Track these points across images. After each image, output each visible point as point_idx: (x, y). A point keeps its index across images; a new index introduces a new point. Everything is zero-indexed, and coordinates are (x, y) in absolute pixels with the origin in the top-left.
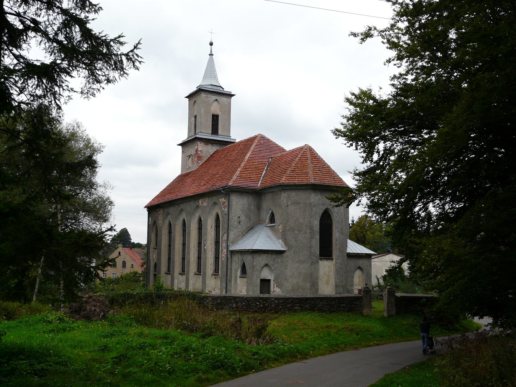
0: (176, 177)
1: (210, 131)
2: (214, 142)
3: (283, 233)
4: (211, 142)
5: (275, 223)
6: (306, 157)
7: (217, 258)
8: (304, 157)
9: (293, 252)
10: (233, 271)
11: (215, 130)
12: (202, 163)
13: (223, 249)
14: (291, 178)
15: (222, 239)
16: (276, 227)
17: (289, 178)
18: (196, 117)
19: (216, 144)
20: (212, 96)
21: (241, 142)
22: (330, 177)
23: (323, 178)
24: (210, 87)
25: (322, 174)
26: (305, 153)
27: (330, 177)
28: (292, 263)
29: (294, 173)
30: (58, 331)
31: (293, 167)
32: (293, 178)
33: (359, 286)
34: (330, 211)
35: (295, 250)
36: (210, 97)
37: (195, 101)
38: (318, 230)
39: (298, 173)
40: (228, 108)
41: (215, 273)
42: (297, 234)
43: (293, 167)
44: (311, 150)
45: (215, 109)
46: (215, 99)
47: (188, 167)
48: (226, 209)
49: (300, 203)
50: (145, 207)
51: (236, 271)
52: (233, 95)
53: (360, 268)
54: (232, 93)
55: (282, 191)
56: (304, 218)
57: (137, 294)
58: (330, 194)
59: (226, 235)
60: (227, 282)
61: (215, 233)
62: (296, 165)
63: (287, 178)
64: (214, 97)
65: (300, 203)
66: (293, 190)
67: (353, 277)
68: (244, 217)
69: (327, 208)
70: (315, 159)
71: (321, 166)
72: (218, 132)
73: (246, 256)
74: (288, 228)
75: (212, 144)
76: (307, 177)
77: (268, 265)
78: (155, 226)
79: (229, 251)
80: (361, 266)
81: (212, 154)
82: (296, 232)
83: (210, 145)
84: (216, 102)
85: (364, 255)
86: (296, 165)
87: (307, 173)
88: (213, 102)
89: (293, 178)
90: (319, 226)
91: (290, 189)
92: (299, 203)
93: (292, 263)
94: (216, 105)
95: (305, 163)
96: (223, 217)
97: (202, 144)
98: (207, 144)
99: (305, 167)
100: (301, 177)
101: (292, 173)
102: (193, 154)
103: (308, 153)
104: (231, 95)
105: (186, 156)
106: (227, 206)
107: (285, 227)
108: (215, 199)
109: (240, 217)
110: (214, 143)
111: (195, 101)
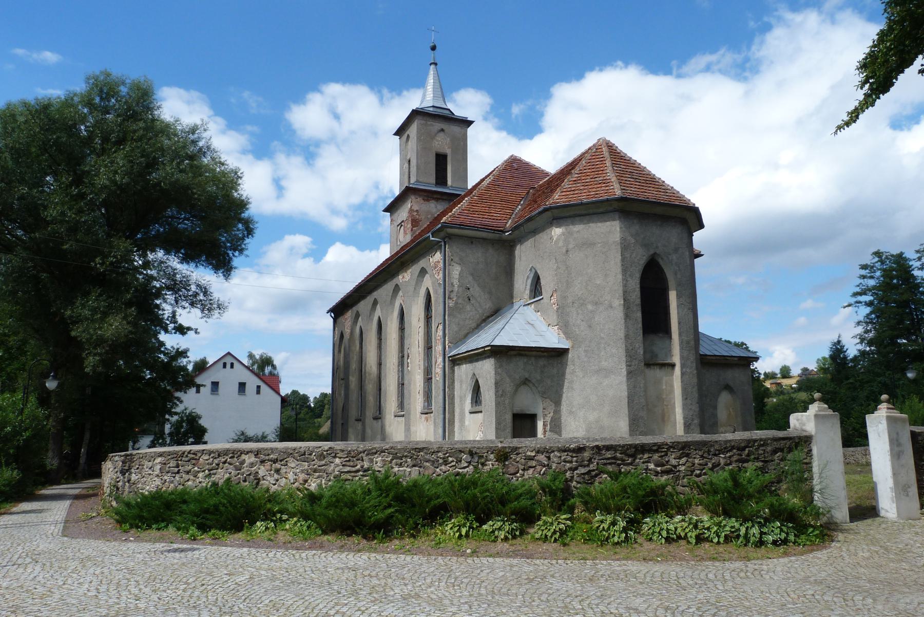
1: (433, 180)
2: (439, 197)
3: (560, 311)
4: (435, 196)
6: (602, 156)
7: (428, 380)
8: (597, 157)
9: (586, 351)
10: (457, 401)
11: (441, 178)
12: (419, 231)
13: (438, 356)
14: (572, 193)
17: (568, 193)
18: (409, 161)
19: (443, 200)
20: (434, 123)
22: (657, 190)
23: (642, 190)
24: (431, 109)
27: (657, 190)
31: (577, 175)
32: (576, 192)
34: (662, 259)
35: (589, 346)
36: (433, 126)
37: (408, 136)
38: (638, 301)
39: (586, 184)
40: (462, 143)
41: (426, 411)
42: (592, 312)
43: (577, 175)
44: (611, 148)
45: (442, 144)
48: (441, 275)
49: (594, 244)
51: (462, 399)
53: (728, 388)
55: (555, 221)
56: (606, 276)
57: (563, 492)
59: (441, 327)
60: (448, 423)
61: (426, 330)
62: (581, 172)
63: (564, 194)
64: (438, 125)
65: (594, 244)
66: (577, 218)
67: (715, 408)
68: (478, 289)
69: (655, 253)
73: (479, 364)
74: (570, 300)
75: (437, 200)
76: (607, 188)
77: (529, 381)
79: (447, 359)
80: (731, 384)
81: (436, 215)
82: (590, 307)
84: (441, 134)
85: (736, 359)
86: (581, 172)
87: (606, 182)
88: (436, 135)
89: (576, 192)
90: (639, 292)
91: (570, 217)
92: (592, 244)
93: (583, 377)
94: (442, 137)
95: (601, 166)
97: (418, 200)
98: (428, 200)
99: (600, 172)
100: (594, 190)
103: (605, 149)
104: (468, 123)
107: (565, 298)
109: (469, 289)
110: (440, 199)
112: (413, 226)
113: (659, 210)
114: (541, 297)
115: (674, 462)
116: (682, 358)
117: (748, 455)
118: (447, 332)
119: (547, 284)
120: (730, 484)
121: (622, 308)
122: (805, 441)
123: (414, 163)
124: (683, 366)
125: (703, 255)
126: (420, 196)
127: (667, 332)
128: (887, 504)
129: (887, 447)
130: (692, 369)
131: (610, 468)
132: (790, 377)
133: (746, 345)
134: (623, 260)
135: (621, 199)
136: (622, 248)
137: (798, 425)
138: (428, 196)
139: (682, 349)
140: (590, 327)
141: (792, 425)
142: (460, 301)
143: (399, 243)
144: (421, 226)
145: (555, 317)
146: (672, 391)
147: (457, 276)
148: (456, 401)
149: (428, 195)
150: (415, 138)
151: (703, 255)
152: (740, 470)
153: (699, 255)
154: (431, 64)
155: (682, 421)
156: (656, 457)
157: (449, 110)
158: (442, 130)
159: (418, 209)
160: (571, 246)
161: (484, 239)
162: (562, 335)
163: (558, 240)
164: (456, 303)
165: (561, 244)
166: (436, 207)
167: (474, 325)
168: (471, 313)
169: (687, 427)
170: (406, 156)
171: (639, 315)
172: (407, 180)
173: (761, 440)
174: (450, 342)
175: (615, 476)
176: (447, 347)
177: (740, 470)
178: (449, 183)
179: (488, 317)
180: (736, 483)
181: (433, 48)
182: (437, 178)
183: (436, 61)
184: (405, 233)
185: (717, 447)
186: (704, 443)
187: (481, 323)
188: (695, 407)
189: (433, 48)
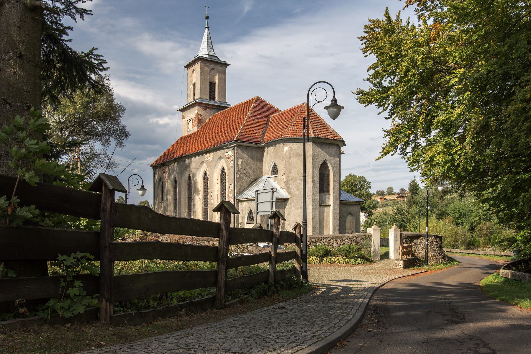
0: (178, 140)
1: (208, 97)
2: (212, 107)
5: (277, 174)
13: (230, 198)
15: (228, 190)
16: (279, 177)
20: (209, 65)
21: (237, 107)
24: (207, 56)
25: (320, 129)
26: (304, 110)
28: (295, 210)
29: (295, 128)
30: (396, 238)
33: (350, 230)
38: (318, 180)
43: (294, 123)
46: (212, 68)
47: (188, 130)
50: (151, 166)
52: (229, 65)
53: (350, 214)
54: (227, 63)
58: (328, 147)
67: (345, 222)
70: (313, 116)
71: (319, 122)
72: (215, 99)
74: (290, 179)
78: (161, 183)
80: (352, 212)
83: (209, 109)
93: (295, 210)
96: (229, 169)
98: (206, 109)
101: (294, 128)
102: (193, 118)
105: (187, 121)
106: (233, 160)
107: (288, 177)
108: (220, 153)
110: (212, 108)
111: (194, 70)
112: (199, 123)
113: (328, 141)
114: (277, 175)
115: (332, 242)
116: (334, 202)
117: (354, 240)
118: (236, 188)
119: (280, 168)
120: (348, 248)
121: (311, 183)
122: (370, 236)
123: (198, 86)
124: (334, 206)
125: (344, 153)
126: (202, 106)
127: (328, 192)
128: (392, 256)
129: (393, 239)
130: (337, 207)
131: (314, 244)
132: (393, 194)
133: (365, 178)
134: (313, 163)
135: (314, 137)
136: (313, 158)
137: (369, 232)
138: (206, 107)
139: (334, 199)
140: (298, 190)
141: (367, 232)
142: (241, 175)
143: (188, 130)
144: (204, 122)
145: (284, 185)
146: (328, 216)
147: (240, 164)
148: (239, 218)
149: (205, 106)
150: (199, 73)
151: (344, 153)
152: (351, 245)
153: (343, 153)
154: (206, 28)
155: (332, 228)
156: (327, 240)
157: (217, 57)
158: (213, 69)
159: (201, 113)
160: (292, 155)
161: (252, 147)
162: (287, 193)
163: (286, 152)
164: (240, 176)
165: (287, 154)
166: (210, 113)
167: (247, 185)
168: (246, 180)
169: (334, 230)
170: (192, 81)
171: (318, 185)
172: (192, 95)
173: (357, 236)
174: (237, 193)
175: (316, 246)
176: (236, 195)
177: (351, 245)
178: (217, 99)
179: (253, 182)
180: (350, 248)
181: (207, 18)
182: (210, 96)
183: (209, 26)
184: (193, 126)
185: (345, 238)
186: (341, 237)
187: (250, 184)
188: (338, 223)
189: (207, 18)
